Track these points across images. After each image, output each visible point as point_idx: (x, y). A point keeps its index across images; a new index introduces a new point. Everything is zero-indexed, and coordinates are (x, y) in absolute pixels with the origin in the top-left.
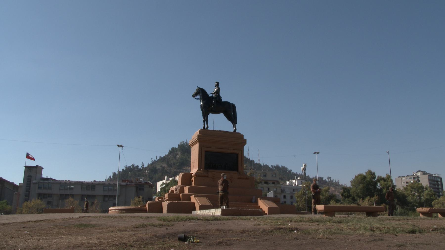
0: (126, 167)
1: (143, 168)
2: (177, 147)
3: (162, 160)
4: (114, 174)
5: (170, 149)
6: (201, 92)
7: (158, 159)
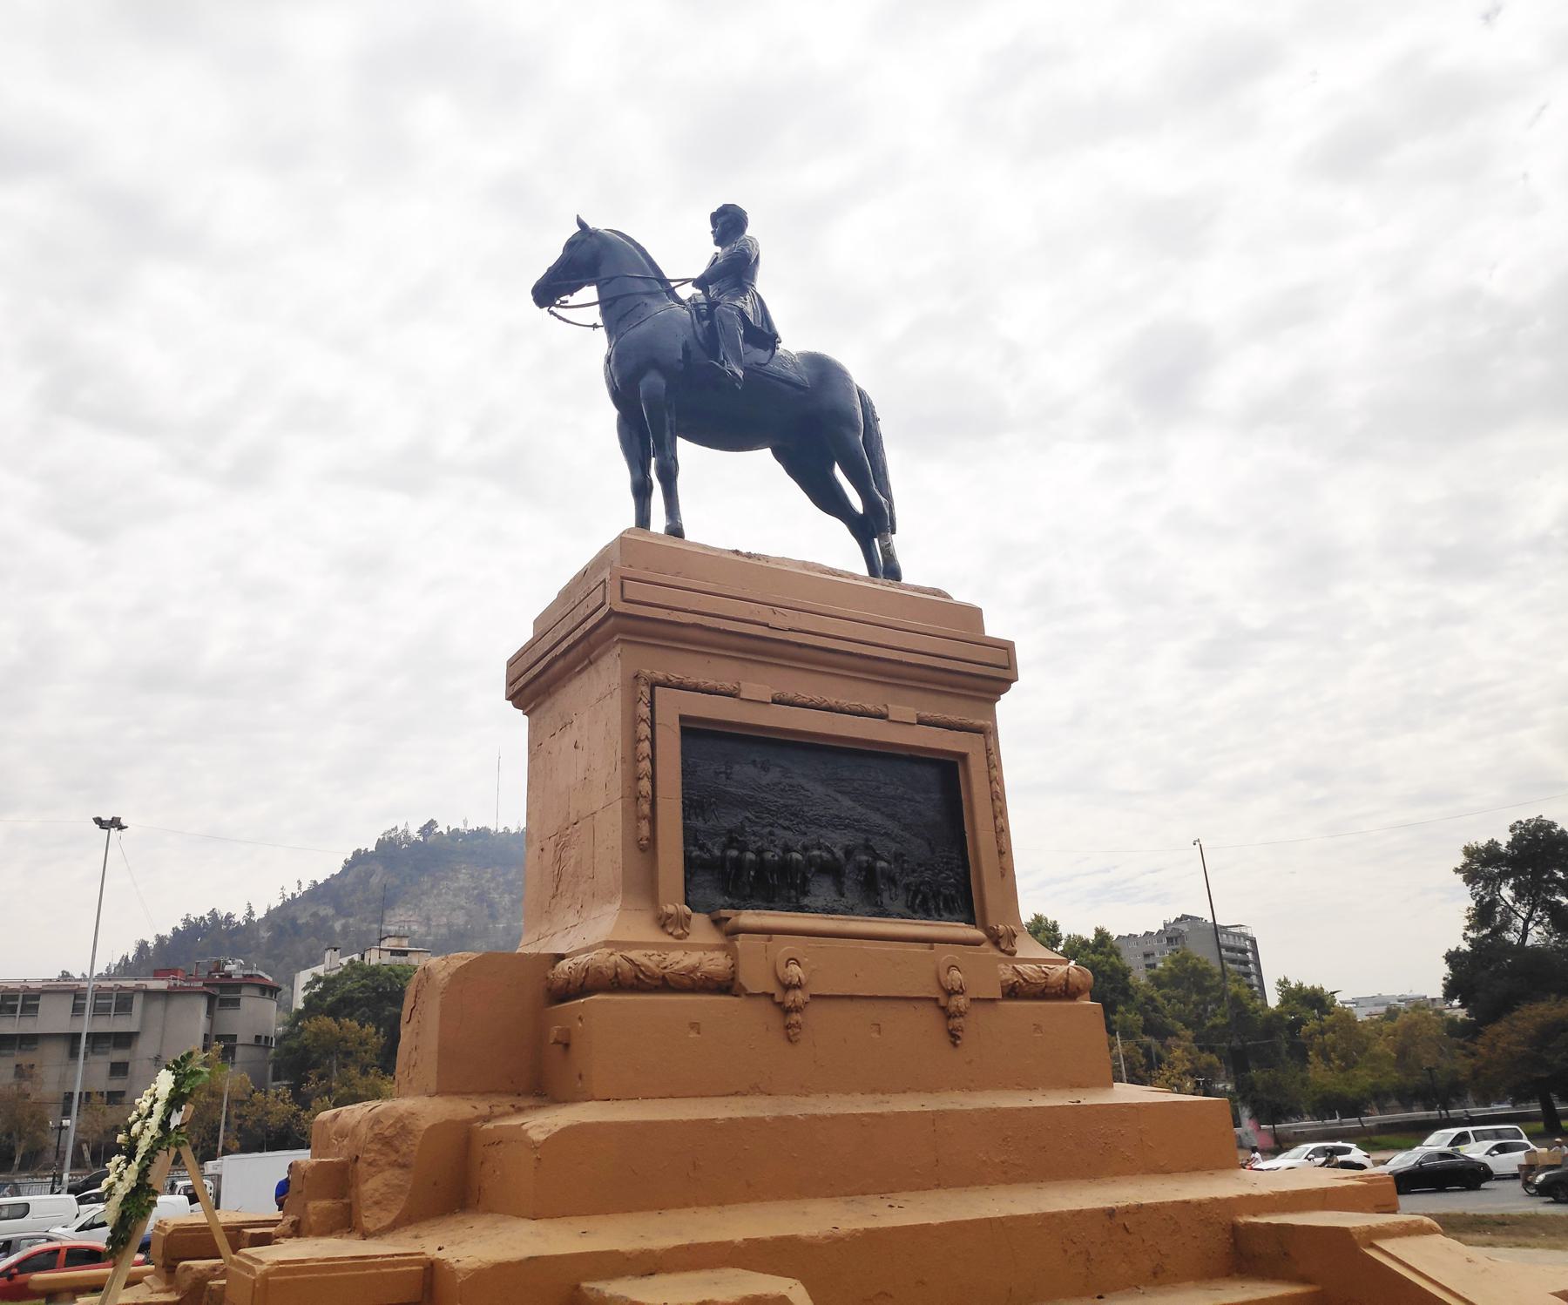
0: (187, 921)
1: (249, 921)
2: (372, 848)
3: (318, 893)
4: (143, 946)
5: (349, 857)
6: (592, 264)
7: (305, 888)
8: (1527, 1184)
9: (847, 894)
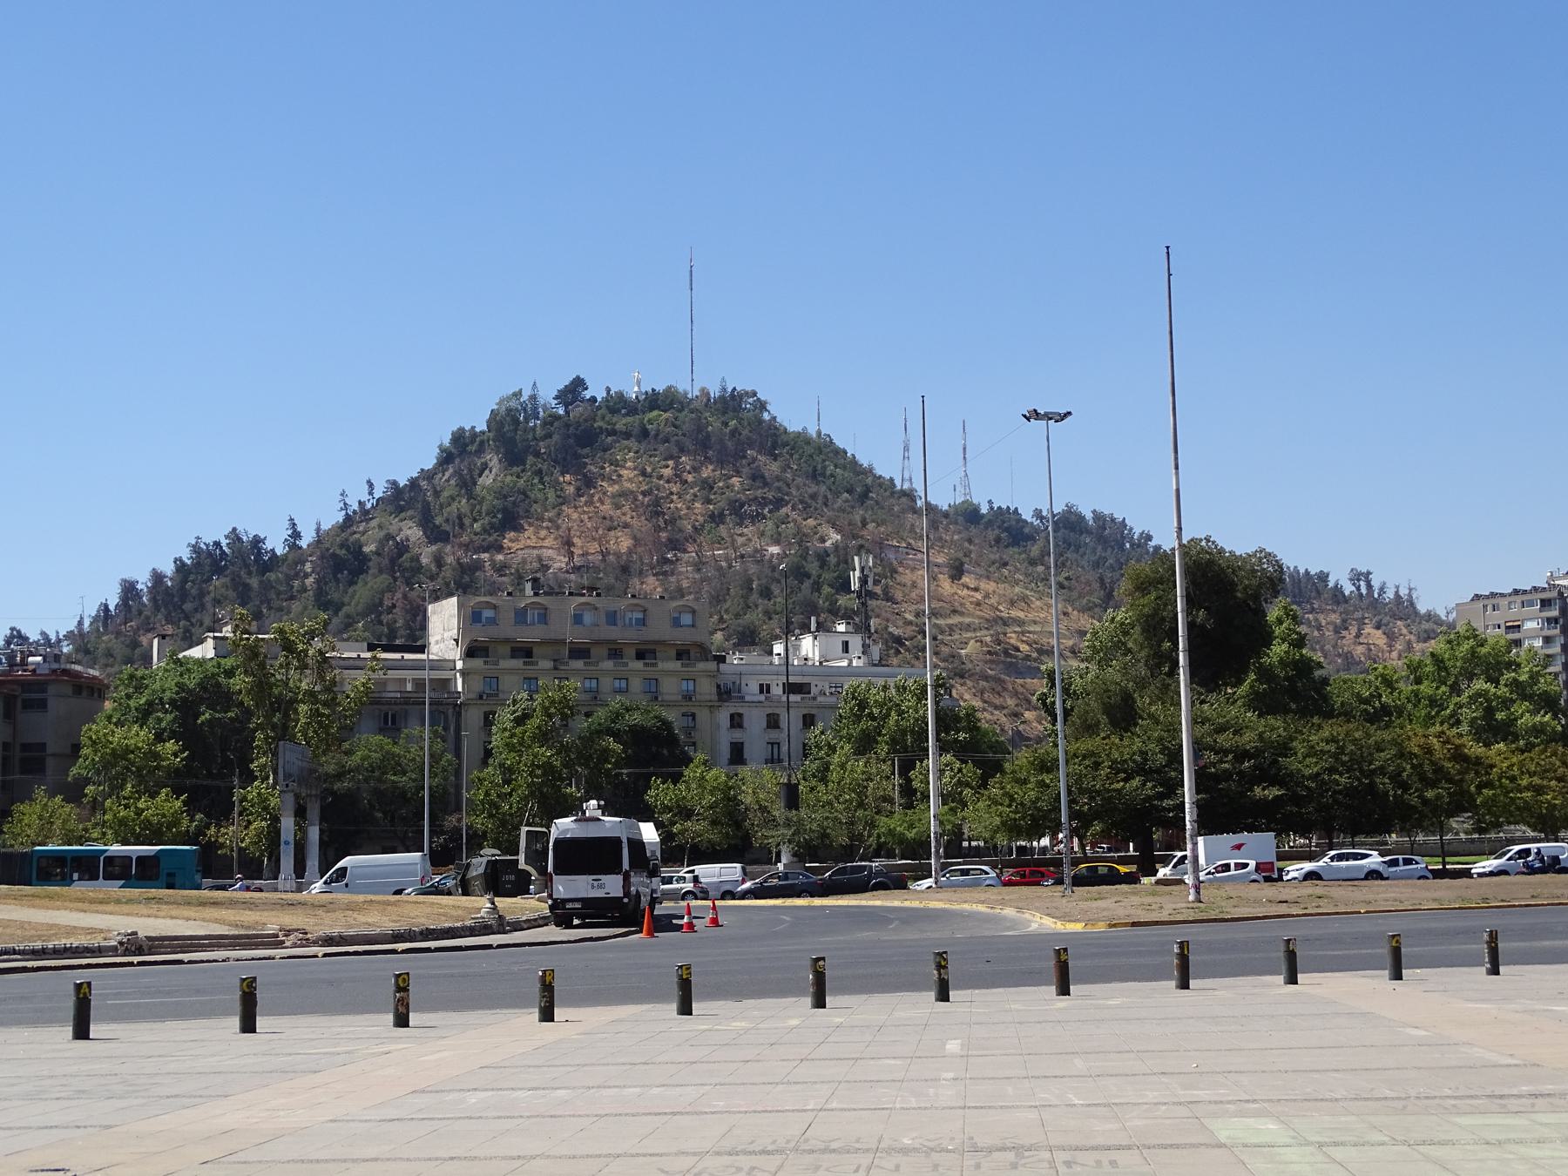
0: (196, 549)
2: (482, 426)
3: (401, 499)
4: (129, 589)
5: (447, 442)
7: (378, 493)
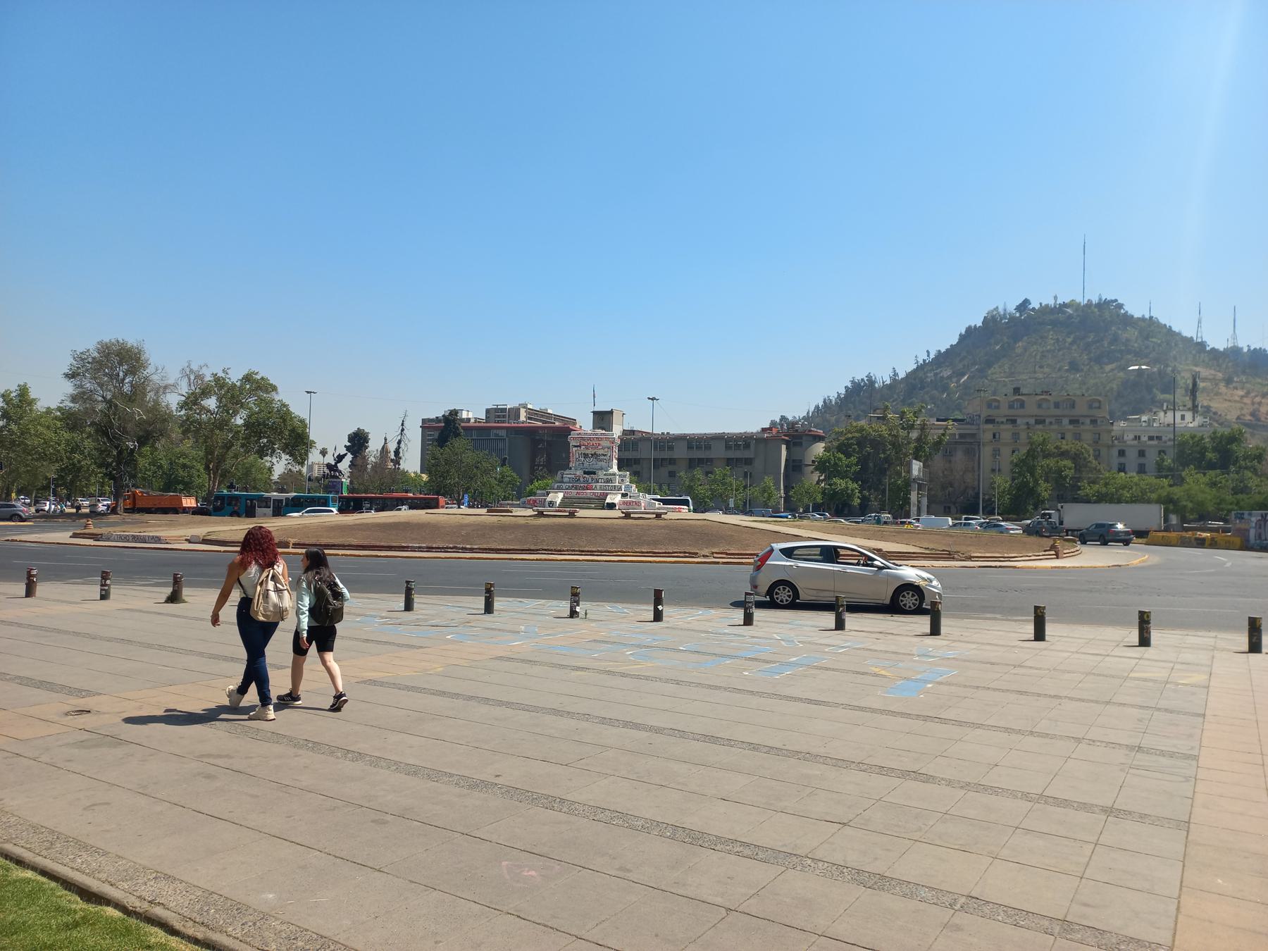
0: (853, 382)
2: (979, 324)
3: (942, 358)
7: (932, 356)
8: (796, 593)
9: (1187, 375)
